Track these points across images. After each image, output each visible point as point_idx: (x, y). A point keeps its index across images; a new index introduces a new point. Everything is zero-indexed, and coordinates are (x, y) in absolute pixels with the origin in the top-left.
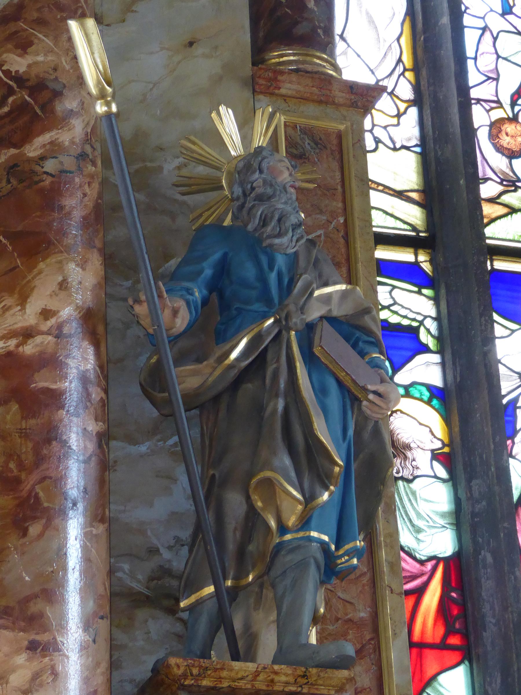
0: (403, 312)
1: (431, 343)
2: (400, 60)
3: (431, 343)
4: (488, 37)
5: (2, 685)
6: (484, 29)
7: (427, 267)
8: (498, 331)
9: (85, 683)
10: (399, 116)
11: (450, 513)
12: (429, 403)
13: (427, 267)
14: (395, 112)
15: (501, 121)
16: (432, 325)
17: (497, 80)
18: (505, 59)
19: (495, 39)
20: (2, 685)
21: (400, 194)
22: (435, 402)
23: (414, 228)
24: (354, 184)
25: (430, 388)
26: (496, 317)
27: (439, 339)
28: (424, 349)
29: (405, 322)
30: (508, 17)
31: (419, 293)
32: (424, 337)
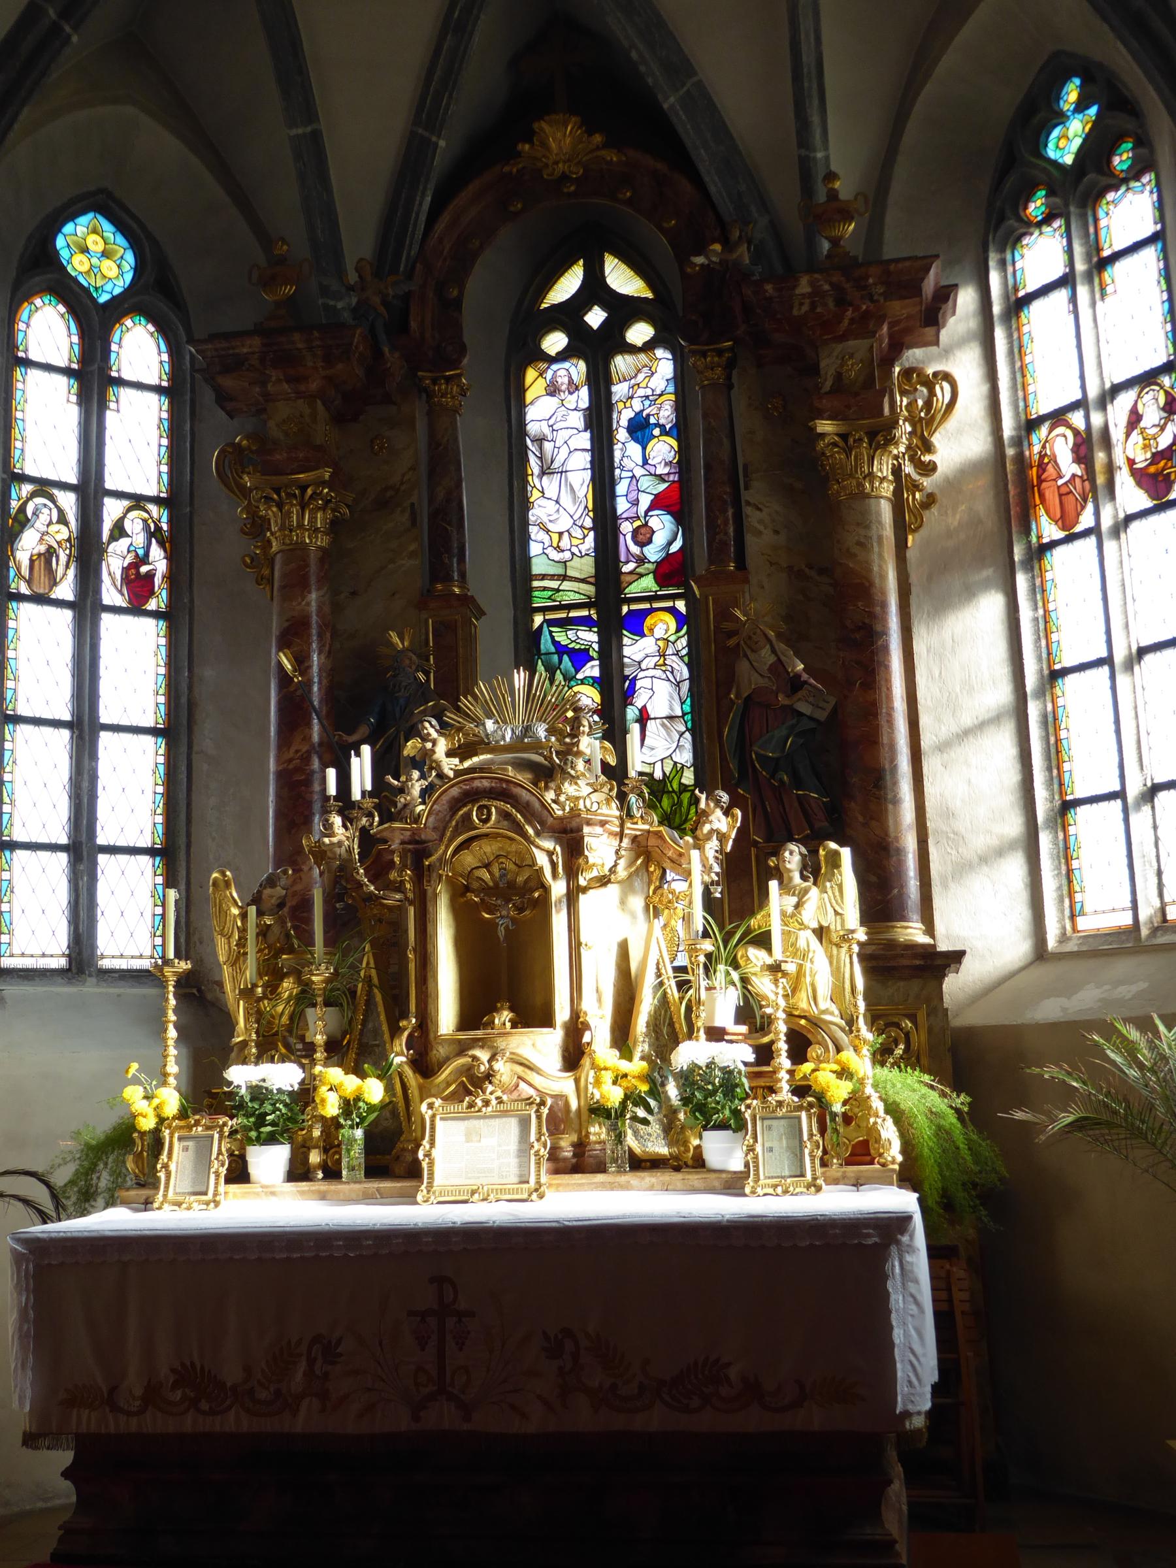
0: (582, 642)
1: (595, 655)
2: (586, 507)
3: (595, 655)
4: (634, 481)
5: (1162, 923)
6: (632, 477)
7: (595, 617)
8: (626, 641)
9: (874, 669)
10: (585, 537)
11: (468, 849)
12: (592, 686)
13: (595, 617)
14: (581, 537)
15: (639, 527)
16: (596, 646)
17: (638, 504)
18: (643, 491)
19: (638, 481)
20: (1162, 923)
21: (583, 581)
22: (595, 685)
23: (589, 597)
24: (680, 392)
25: (593, 678)
26: (625, 632)
27: (599, 652)
28: (592, 659)
29: (583, 647)
30: (646, 467)
31: (590, 631)
32: (592, 653)
